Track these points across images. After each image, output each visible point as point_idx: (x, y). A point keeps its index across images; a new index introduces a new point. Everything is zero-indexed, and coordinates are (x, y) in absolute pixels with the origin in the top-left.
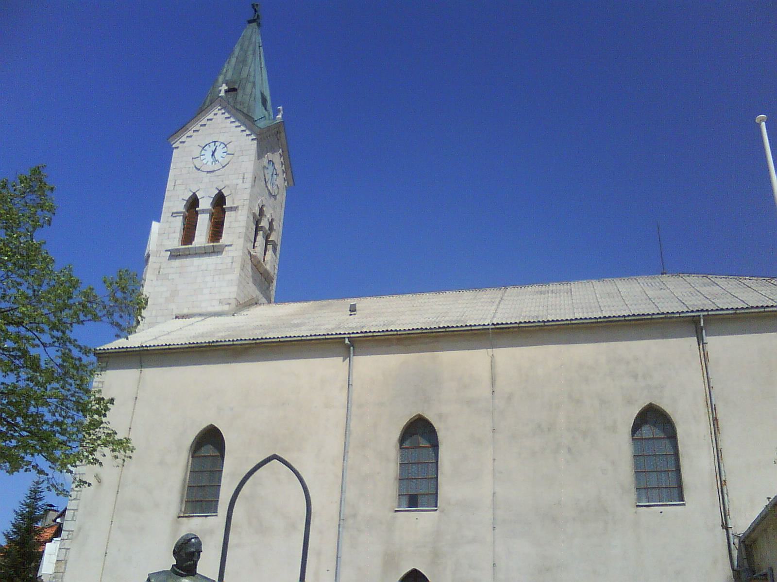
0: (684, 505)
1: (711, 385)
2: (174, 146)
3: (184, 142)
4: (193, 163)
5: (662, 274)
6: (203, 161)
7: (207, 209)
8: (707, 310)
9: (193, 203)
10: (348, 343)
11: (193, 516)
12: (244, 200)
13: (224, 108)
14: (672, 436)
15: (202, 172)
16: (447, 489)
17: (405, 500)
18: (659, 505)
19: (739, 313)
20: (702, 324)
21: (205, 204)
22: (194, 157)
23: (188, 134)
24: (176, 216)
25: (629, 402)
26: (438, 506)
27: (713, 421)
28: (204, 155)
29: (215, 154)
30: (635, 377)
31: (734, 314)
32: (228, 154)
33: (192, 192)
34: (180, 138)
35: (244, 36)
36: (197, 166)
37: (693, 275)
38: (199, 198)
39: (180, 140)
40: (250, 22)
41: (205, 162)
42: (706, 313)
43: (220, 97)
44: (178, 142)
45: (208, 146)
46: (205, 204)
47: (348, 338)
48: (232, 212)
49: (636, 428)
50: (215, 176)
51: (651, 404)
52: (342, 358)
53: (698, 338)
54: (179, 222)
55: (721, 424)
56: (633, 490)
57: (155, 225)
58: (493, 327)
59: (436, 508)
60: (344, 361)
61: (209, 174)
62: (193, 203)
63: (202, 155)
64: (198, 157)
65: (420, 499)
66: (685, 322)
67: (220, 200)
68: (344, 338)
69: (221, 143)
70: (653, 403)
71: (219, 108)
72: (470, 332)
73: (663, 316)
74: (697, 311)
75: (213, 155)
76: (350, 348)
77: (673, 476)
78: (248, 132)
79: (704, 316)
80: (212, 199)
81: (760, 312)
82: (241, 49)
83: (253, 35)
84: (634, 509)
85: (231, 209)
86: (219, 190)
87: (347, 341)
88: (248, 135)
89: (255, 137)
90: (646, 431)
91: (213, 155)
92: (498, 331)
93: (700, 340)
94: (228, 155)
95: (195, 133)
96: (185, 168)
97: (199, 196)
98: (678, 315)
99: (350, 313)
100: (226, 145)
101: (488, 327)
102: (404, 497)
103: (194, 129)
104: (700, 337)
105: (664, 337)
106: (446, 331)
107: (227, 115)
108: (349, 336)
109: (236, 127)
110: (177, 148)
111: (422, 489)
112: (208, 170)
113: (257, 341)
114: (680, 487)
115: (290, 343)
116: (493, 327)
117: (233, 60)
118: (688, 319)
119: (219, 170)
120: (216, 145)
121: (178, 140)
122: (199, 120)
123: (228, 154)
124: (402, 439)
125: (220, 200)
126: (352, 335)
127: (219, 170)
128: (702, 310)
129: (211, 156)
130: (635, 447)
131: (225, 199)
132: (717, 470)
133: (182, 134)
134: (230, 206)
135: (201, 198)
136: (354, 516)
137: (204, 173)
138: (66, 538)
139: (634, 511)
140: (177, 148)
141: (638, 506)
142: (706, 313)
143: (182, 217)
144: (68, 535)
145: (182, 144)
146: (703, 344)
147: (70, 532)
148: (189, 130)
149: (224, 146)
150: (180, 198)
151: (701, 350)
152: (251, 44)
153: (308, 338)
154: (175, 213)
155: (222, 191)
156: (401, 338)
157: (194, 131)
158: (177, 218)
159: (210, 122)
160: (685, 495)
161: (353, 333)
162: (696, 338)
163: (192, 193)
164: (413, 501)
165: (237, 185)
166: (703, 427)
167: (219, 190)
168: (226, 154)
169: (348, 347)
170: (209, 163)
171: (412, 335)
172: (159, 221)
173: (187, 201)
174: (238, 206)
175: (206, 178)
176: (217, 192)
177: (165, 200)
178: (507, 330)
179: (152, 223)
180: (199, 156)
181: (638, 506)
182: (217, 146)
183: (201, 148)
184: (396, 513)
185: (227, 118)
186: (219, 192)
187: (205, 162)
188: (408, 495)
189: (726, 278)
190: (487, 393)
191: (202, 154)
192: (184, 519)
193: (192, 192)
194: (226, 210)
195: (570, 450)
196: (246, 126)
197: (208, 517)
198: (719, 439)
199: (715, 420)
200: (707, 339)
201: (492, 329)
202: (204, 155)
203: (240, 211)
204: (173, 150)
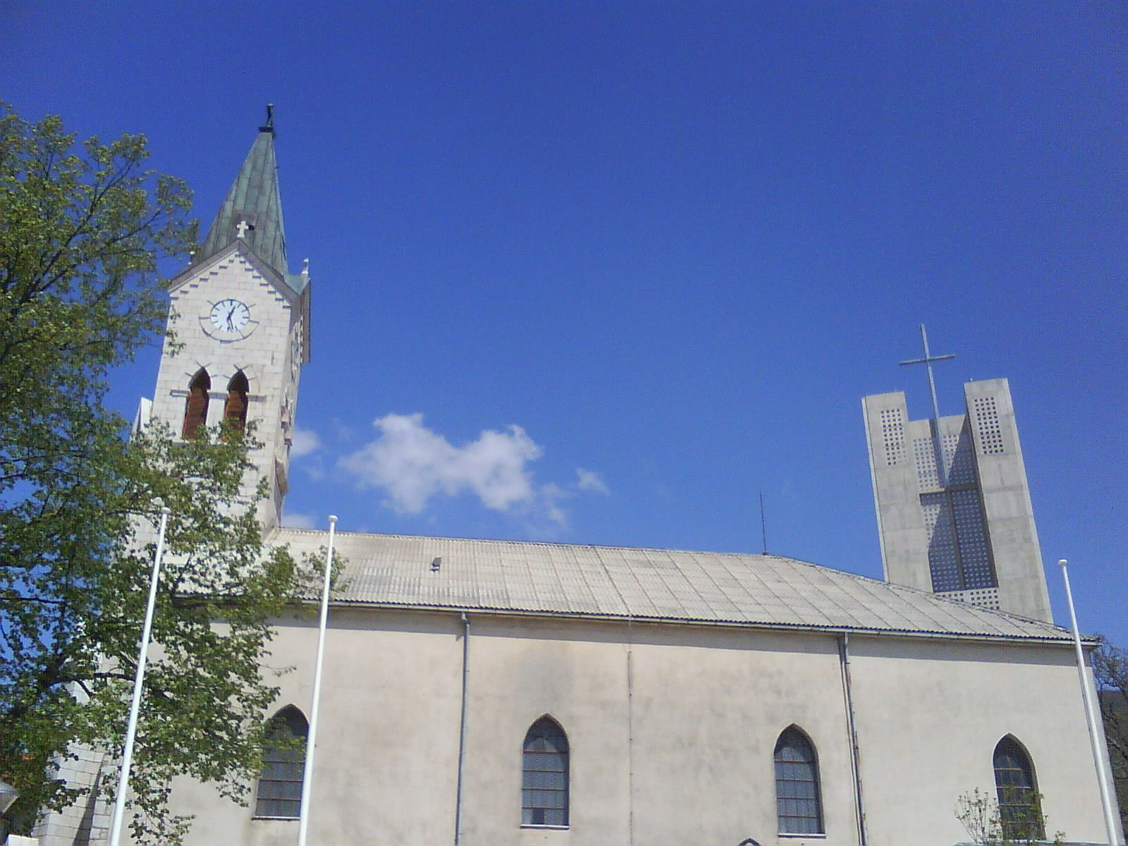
0: (824, 837)
1: (853, 711)
2: (171, 295)
3: (186, 292)
4: (200, 324)
5: (765, 554)
6: (215, 324)
7: (222, 394)
8: (851, 628)
9: (201, 381)
10: (465, 619)
11: (273, 819)
12: (274, 388)
13: (245, 255)
14: (812, 761)
15: (214, 341)
16: (579, 806)
17: (529, 817)
18: (787, 837)
19: (883, 635)
20: (846, 642)
21: (219, 385)
22: (202, 316)
23: (192, 282)
24: (176, 396)
25: (772, 720)
26: (570, 823)
27: (854, 749)
28: (216, 316)
29: (232, 318)
30: (779, 693)
31: (878, 634)
32: (251, 321)
33: (199, 365)
34: (181, 286)
35: (256, 149)
36: (206, 330)
37: (799, 562)
38: (210, 375)
39: (181, 289)
40: (263, 130)
41: (217, 325)
42: (851, 631)
43: (239, 239)
44: (178, 291)
45: (221, 304)
46: (219, 385)
47: (465, 612)
48: (257, 403)
49: (778, 750)
50: (233, 348)
51: (793, 725)
52: (454, 636)
53: (841, 657)
54: (180, 405)
55: (861, 751)
56: (776, 818)
57: (145, 404)
58: (633, 619)
59: (567, 827)
60: (457, 640)
61: (223, 345)
62: (201, 381)
63: (213, 316)
64: (207, 318)
65: (547, 815)
66: (829, 636)
67: (239, 384)
68: (461, 612)
69: (240, 304)
70: (796, 724)
71: (237, 253)
72: (606, 622)
73: (809, 628)
74: (842, 627)
75: (229, 318)
76: (465, 624)
77: (812, 804)
78: (279, 296)
79: (848, 633)
80: (229, 380)
81: (902, 636)
82: (254, 168)
83: (264, 142)
84: (776, 839)
85: (256, 398)
86: (239, 370)
87: (464, 617)
88: (270, 292)
89: (288, 305)
90: (787, 753)
91: (229, 318)
92: (638, 624)
93: (843, 658)
94: (250, 323)
95: (202, 283)
96: (188, 329)
97: (210, 372)
98: (824, 630)
99: (432, 567)
100: (247, 309)
101: (627, 618)
102: (528, 811)
103: (201, 276)
104: (843, 656)
105: (807, 651)
106: (581, 618)
107: (248, 265)
108: (466, 610)
109: (261, 285)
110: (176, 299)
111: (550, 801)
112: (223, 339)
113: (352, 604)
114: (566, 810)
115: (392, 611)
116: (633, 619)
117: (244, 183)
118: (832, 634)
119: (238, 340)
120: (233, 305)
121: (177, 289)
122: (208, 265)
123: (251, 321)
124: (526, 743)
125: (239, 384)
126: (470, 610)
127: (238, 340)
128: (847, 627)
129: (226, 320)
130: (776, 769)
131: (248, 384)
132: (857, 803)
133: (185, 280)
134: (255, 394)
135: (213, 377)
136: (473, 830)
137: (216, 341)
138: (98, 837)
139: (776, 842)
140: (176, 299)
141: (780, 836)
142: (851, 631)
143: (185, 399)
144: (100, 834)
145: (183, 295)
146: (846, 663)
147: (104, 830)
148: (195, 278)
149: (244, 308)
150: (183, 372)
151: (844, 670)
152: (268, 163)
153: (416, 607)
154: (175, 391)
155: (244, 371)
156: (526, 620)
157: (201, 279)
158: (178, 398)
159: (224, 270)
160: (826, 826)
161: (471, 608)
162: (838, 656)
163: (200, 368)
164: (538, 817)
165: (264, 366)
166: (845, 756)
167: (239, 370)
168: (247, 320)
169: (464, 624)
170: (225, 329)
171: (539, 618)
172: (151, 398)
173: (193, 377)
174: (266, 396)
175: (221, 349)
176: (235, 371)
177: (160, 371)
178: (647, 624)
179: (140, 401)
180: (208, 316)
181: (780, 836)
182: (234, 308)
183: (212, 306)
184: (523, 830)
185: (247, 270)
186: (238, 373)
187: (217, 325)
188: (532, 808)
189: (837, 573)
190: (623, 696)
191: (213, 313)
192: (260, 821)
193: (199, 365)
194: (249, 399)
195: (711, 769)
196: (275, 286)
197: (292, 822)
198: (860, 768)
199: (856, 748)
200: (850, 658)
201: (632, 621)
202: (216, 316)
203: (268, 404)
204: (170, 300)
